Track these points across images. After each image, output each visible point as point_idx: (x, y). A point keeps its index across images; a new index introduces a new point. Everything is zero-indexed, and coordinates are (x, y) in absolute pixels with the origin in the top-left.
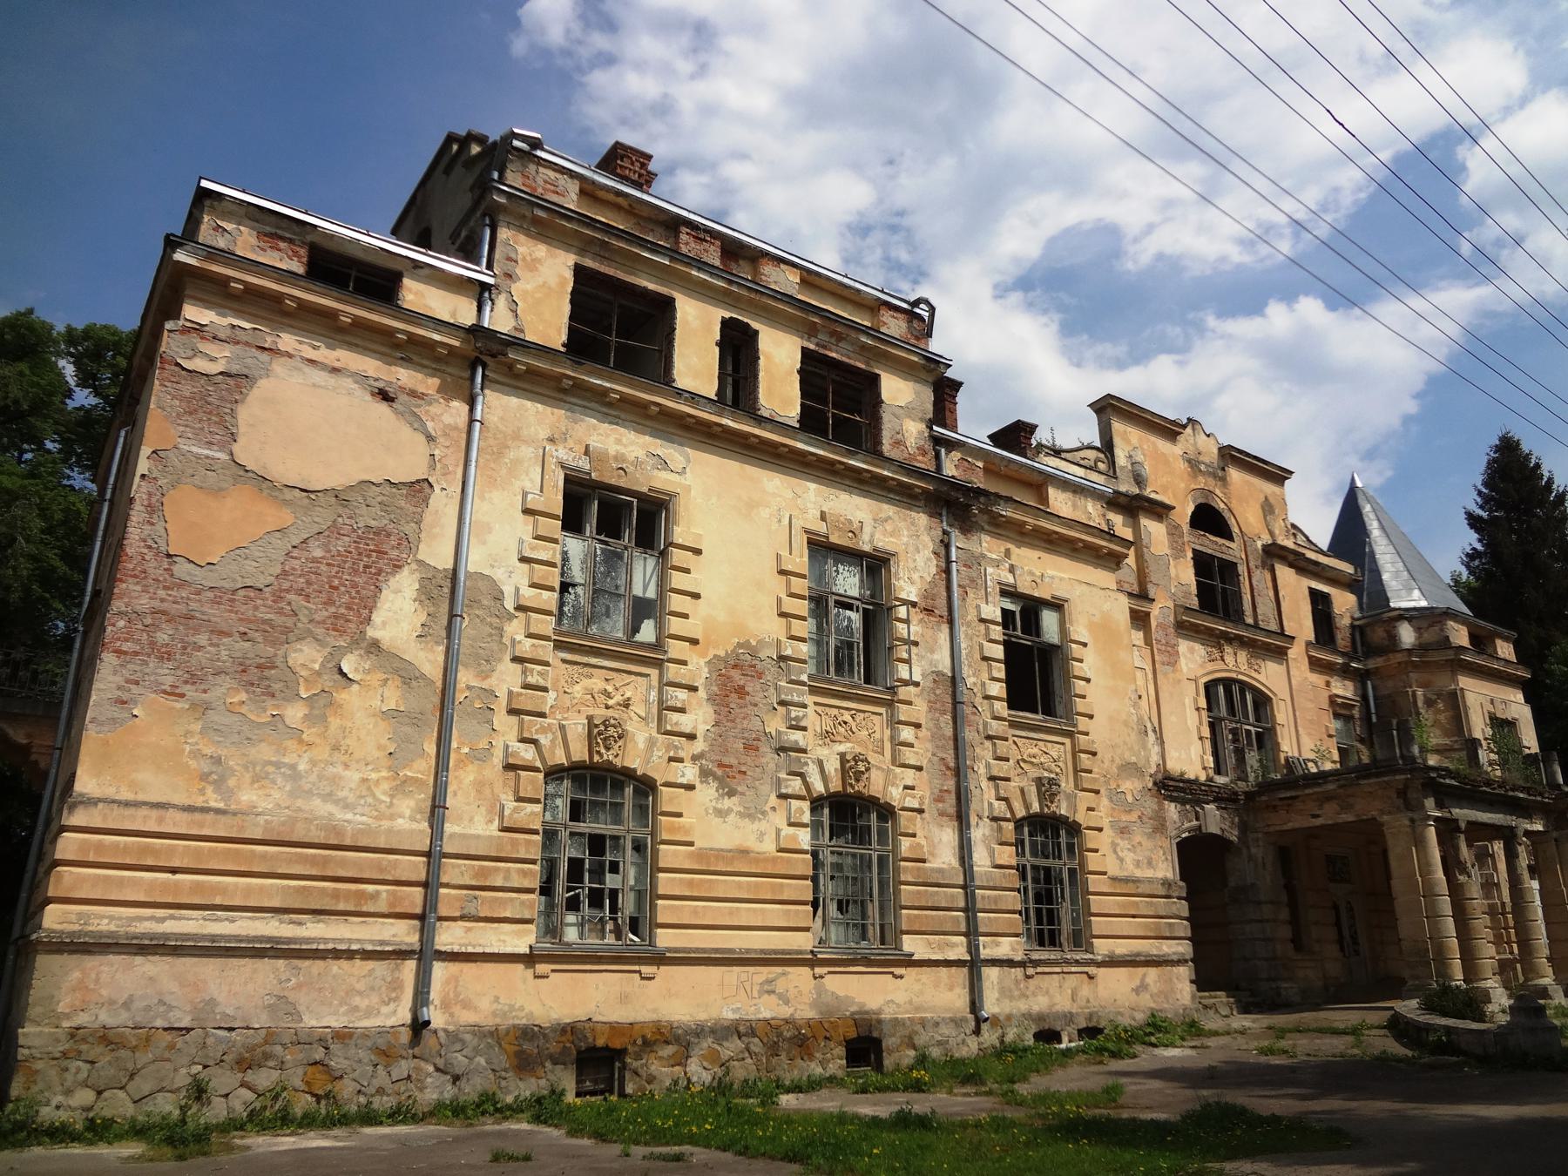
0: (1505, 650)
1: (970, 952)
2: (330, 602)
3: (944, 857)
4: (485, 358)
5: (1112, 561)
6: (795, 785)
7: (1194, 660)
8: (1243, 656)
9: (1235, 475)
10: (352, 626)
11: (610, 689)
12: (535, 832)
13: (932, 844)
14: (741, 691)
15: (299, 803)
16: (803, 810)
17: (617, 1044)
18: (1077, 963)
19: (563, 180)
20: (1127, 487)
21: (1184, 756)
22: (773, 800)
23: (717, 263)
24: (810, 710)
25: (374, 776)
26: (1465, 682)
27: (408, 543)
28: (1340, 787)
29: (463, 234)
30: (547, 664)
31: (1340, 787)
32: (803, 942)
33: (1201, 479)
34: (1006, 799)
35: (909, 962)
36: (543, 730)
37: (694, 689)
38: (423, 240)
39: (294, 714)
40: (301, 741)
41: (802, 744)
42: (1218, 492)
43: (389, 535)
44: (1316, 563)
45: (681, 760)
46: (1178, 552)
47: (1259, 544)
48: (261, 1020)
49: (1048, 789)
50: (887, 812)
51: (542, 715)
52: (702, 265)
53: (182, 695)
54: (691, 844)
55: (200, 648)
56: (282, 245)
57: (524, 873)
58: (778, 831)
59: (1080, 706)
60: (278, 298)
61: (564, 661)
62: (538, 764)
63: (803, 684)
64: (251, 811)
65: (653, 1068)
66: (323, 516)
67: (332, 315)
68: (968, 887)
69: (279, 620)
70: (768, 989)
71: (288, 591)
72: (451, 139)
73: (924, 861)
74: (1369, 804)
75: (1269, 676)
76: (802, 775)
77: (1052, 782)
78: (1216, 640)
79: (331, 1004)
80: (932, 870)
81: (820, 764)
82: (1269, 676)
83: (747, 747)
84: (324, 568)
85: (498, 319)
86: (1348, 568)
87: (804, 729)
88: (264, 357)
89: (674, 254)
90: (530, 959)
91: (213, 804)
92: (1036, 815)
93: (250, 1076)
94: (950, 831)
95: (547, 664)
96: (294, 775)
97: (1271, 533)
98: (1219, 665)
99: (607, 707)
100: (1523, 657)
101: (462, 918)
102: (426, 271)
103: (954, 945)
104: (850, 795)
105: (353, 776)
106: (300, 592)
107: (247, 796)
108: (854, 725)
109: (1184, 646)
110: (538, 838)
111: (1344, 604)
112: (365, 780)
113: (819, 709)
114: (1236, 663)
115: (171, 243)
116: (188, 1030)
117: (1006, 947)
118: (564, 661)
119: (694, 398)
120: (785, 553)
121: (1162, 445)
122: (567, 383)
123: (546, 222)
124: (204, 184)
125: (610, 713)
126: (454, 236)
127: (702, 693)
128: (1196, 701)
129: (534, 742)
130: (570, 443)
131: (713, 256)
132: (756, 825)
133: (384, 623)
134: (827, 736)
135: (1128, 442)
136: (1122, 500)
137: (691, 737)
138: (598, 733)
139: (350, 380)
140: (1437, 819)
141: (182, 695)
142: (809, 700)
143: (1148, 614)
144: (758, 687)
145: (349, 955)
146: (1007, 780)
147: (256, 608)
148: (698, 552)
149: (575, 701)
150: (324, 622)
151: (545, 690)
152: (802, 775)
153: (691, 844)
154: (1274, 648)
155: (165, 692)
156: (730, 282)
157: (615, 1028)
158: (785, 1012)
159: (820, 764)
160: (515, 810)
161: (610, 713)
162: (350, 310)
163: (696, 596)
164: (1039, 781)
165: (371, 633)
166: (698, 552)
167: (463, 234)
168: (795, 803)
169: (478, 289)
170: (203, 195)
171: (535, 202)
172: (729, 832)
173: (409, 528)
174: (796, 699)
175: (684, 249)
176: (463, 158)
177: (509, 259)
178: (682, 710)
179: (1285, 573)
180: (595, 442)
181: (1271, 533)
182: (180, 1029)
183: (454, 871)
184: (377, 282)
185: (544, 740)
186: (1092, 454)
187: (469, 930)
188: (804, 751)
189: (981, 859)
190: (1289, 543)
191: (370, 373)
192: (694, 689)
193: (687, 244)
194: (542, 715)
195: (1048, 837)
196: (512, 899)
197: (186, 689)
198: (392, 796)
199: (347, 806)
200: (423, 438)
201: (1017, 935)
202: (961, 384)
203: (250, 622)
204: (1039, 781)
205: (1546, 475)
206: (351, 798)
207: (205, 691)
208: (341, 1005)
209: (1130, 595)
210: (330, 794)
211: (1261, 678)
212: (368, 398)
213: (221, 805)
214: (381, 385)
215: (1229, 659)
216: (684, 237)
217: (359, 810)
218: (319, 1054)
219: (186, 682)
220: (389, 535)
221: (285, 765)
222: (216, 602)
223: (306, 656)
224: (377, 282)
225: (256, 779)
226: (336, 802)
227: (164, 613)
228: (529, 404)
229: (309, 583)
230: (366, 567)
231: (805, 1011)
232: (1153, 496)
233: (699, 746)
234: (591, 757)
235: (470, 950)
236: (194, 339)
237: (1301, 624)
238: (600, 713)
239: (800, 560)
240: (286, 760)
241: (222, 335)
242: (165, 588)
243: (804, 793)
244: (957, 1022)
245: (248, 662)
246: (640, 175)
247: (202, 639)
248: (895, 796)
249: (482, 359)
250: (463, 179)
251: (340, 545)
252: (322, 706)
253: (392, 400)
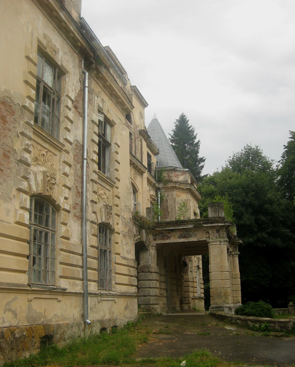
1: (83, 289)
3: (75, 239)
6: (24, 185)
13: (71, 231)
16: (27, 200)
22: (14, 192)
32: (23, 279)
35: (64, 292)
47: (138, 129)
50: (57, 208)
65: (276, 314)
81: (35, 175)
94: (77, 224)
103: (77, 285)
144: (12, 120)
158: (14, 323)
195: (105, 229)
205: (195, 134)
211: (136, 182)
243: (28, 190)
244: (78, 325)
248: (61, 201)
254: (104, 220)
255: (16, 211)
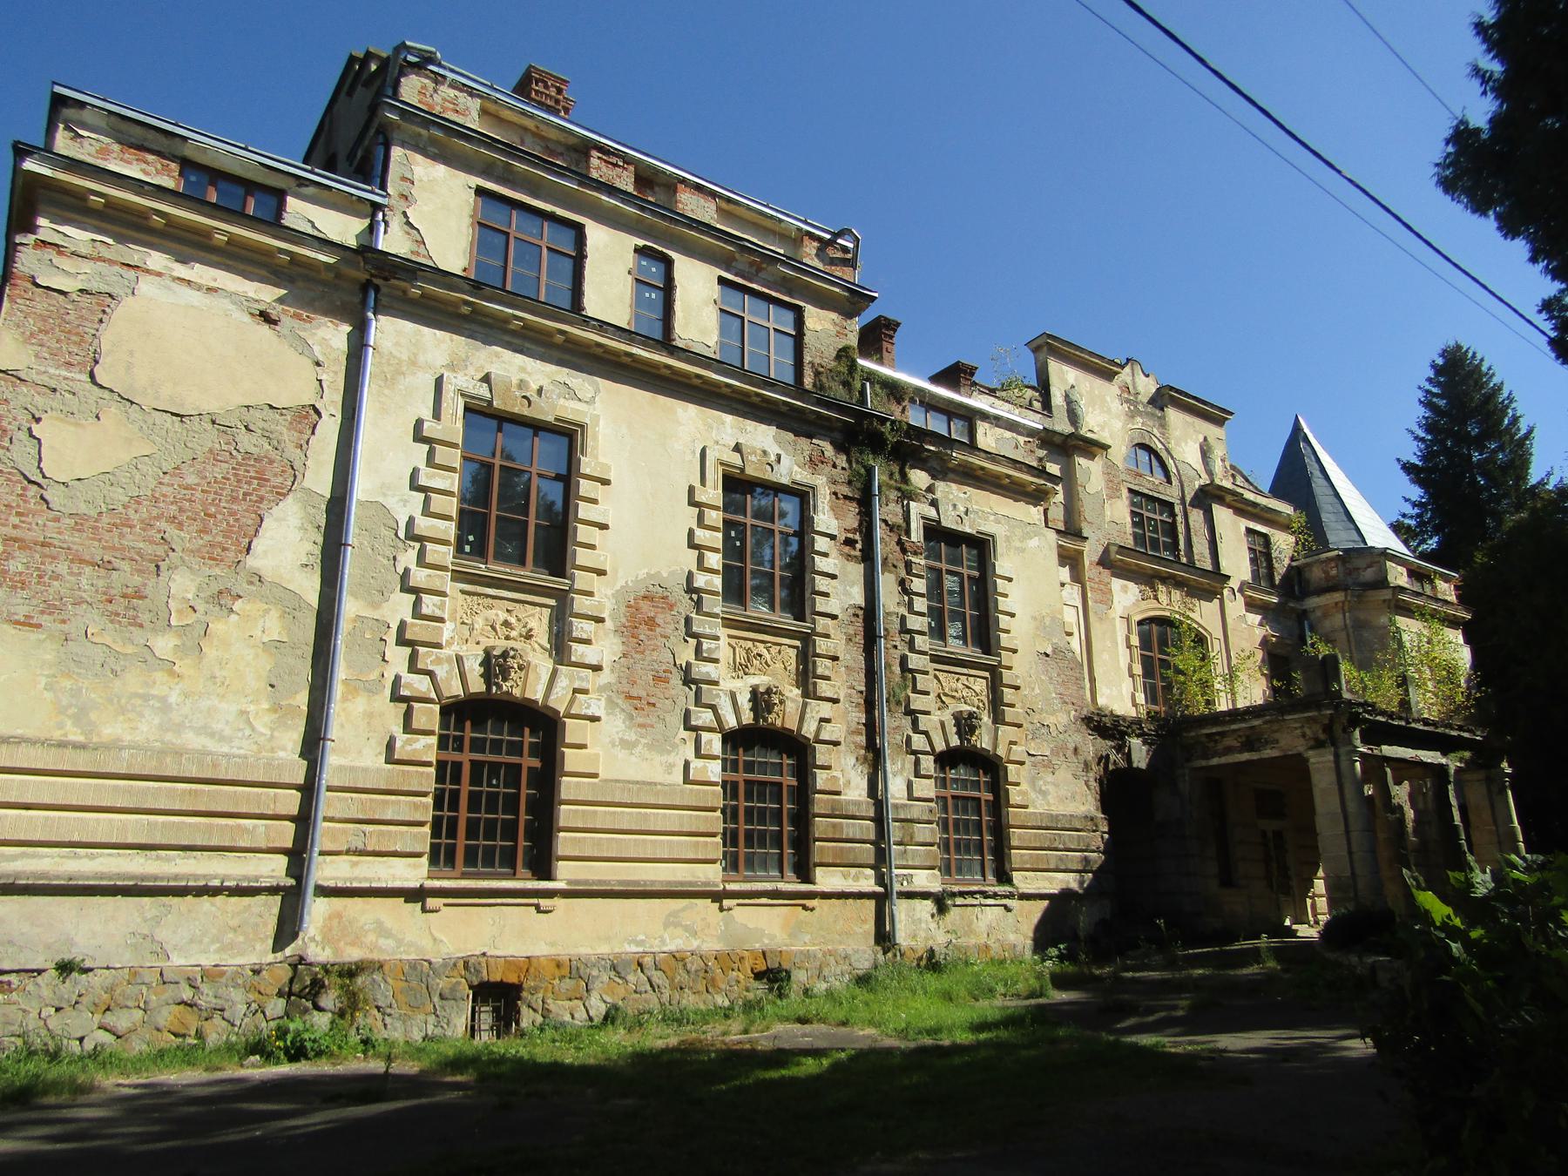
0: (1446, 590)
2: (204, 531)
4: (377, 281)
5: (1038, 497)
7: (1126, 598)
8: (1177, 595)
9: (1172, 414)
10: (232, 555)
11: (513, 620)
12: (428, 764)
13: (842, 775)
14: (651, 623)
15: (169, 737)
17: (512, 978)
18: (995, 896)
19: (463, 98)
20: (1062, 426)
21: (1115, 693)
23: (630, 189)
24: (724, 641)
25: (252, 708)
26: (1402, 621)
27: (294, 472)
28: (1265, 723)
29: (359, 154)
30: (443, 594)
31: (1265, 723)
33: (1139, 419)
34: (926, 733)
36: (438, 661)
37: (600, 620)
38: (330, 165)
39: (164, 645)
40: (172, 673)
41: (714, 676)
42: (1155, 431)
43: (271, 462)
44: (1255, 505)
45: (585, 692)
46: (1114, 493)
48: (126, 959)
49: (966, 724)
51: (438, 646)
52: (612, 190)
53: (39, 626)
54: (595, 776)
55: (56, 577)
56: (151, 158)
57: (416, 806)
58: (687, 765)
59: (1005, 640)
60: (144, 214)
61: (463, 592)
62: (433, 695)
63: (716, 616)
64: (115, 746)
66: (210, 439)
67: (207, 233)
68: (879, 820)
69: (149, 549)
70: (671, 922)
71: (158, 518)
72: (352, 59)
73: (838, 793)
74: (1290, 739)
75: (1204, 614)
76: (713, 708)
77: (971, 715)
78: (1148, 580)
79: (201, 942)
80: (848, 802)
81: (733, 696)
82: (1204, 614)
83: (657, 678)
84: (198, 495)
85: (393, 241)
86: (1286, 508)
87: (716, 661)
88: (132, 274)
89: (586, 180)
90: (416, 895)
91: (71, 737)
92: (956, 749)
93: (110, 1019)
95: (443, 594)
96: (165, 707)
97: (1210, 473)
98: (1153, 603)
99: (507, 638)
100: (1464, 598)
101: (348, 852)
102: (311, 190)
104: (762, 729)
105: (229, 708)
106: (172, 519)
107: (111, 729)
108: (768, 657)
109: (1117, 584)
110: (432, 770)
111: (1284, 544)
112: (243, 713)
113: (733, 642)
114: (1169, 602)
115: (21, 151)
116: (40, 972)
117: (926, 880)
118: (463, 592)
119: (602, 326)
120: (697, 484)
121: (1098, 383)
122: (466, 310)
123: (445, 140)
124: (58, 89)
125: (511, 644)
126: (351, 157)
127: (609, 624)
128: (1128, 639)
129: (430, 674)
130: (471, 371)
131: (626, 182)
132: (664, 758)
133: (265, 552)
134: (741, 669)
135: (1063, 380)
136: (1057, 440)
137: (597, 668)
138: (495, 666)
139: (226, 301)
140: (1362, 755)
141: (39, 626)
142: (723, 633)
143: (1081, 553)
145: (213, 892)
146: (928, 713)
147: (122, 536)
148: (605, 482)
149: (471, 629)
150: (199, 550)
151: (441, 620)
152: (713, 708)
153: (595, 776)
154: (1210, 584)
155: (17, 623)
156: (642, 209)
157: (510, 963)
159: (733, 696)
160: (408, 742)
161: (511, 644)
162: (225, 229)
163: (603, 527)
164: (958, 717)
165: (251, 562)
166: (605, 482)
167: (359, 154)
168: (705, 736)
169: (369, 209)
170: (58, 102)
171: (429, 120)
172: (632, 762)
173: (294, 454)
174: (708, 631)
175: (594, 175)
176: (365, 76)
177: (404, 179)
178: (587, 642)
179: (1222, 514)
180: (495, 370)
181: (1210, 473)
182: (33, 971)
183: (328, 804)
184: (260, 198)
185: (441, 672)
186: (1029, 393)
187: (355, 864)
188: (716, 683)
189: (896, 789)
190: (1227, 484)
191: (251, 295)
192: (600, 620)
193: (598, 168)
194: (438, 646)
195: (973, 768)
196: (402, 833)
197: (45, 620)
198: (272, 730)
199: (222, 739)
200: (308, 363)
201: (932, 868)
202: (898, 324)
203: (113, 548)
204: (958, 717)
206: (227, 732)
207: (64, 622)
208: (212, 942)
209: (1058, 532)
210: (205, 727)
212: (247, 319)
213: (81, 739)
214: (262, 308)
215: (1163, 597)
216: (594, 162)
217: (236, 743)
218: (187, 994)
219: (43, 612)
220: (271, 462)
221: (154, 696)
222: (79, 528)
223: (183, 584)
224: (260, 198)
225: (123, 711)
226: (212, 735)
227: (15, 540)
228: (426, 330)
229: (181, 510)
230: (245, 494)
231: (711, 944)
232: (1089, 435)
233: (605, 677)
234: (489, 688)
235: (355, 885)
236: (50, 253)
237: (1237, 564)
238: (500, 645)
239: (713, 493)
240: (154, 692)
241: (83, 251)
242: (19, 514)
245: (113, 592)
246: (557, 102)
247: (62, 568)
249: (368, 285)
250: (362, 95)
251: (219, 471)
252: (196, 640)
253: (275, 322)
254: (955, 741)
255: (687, 765)
